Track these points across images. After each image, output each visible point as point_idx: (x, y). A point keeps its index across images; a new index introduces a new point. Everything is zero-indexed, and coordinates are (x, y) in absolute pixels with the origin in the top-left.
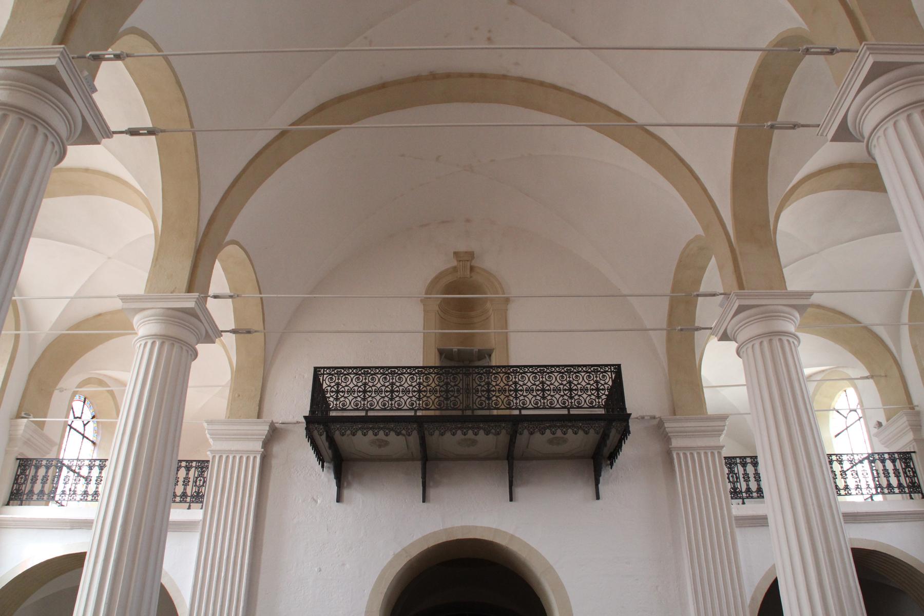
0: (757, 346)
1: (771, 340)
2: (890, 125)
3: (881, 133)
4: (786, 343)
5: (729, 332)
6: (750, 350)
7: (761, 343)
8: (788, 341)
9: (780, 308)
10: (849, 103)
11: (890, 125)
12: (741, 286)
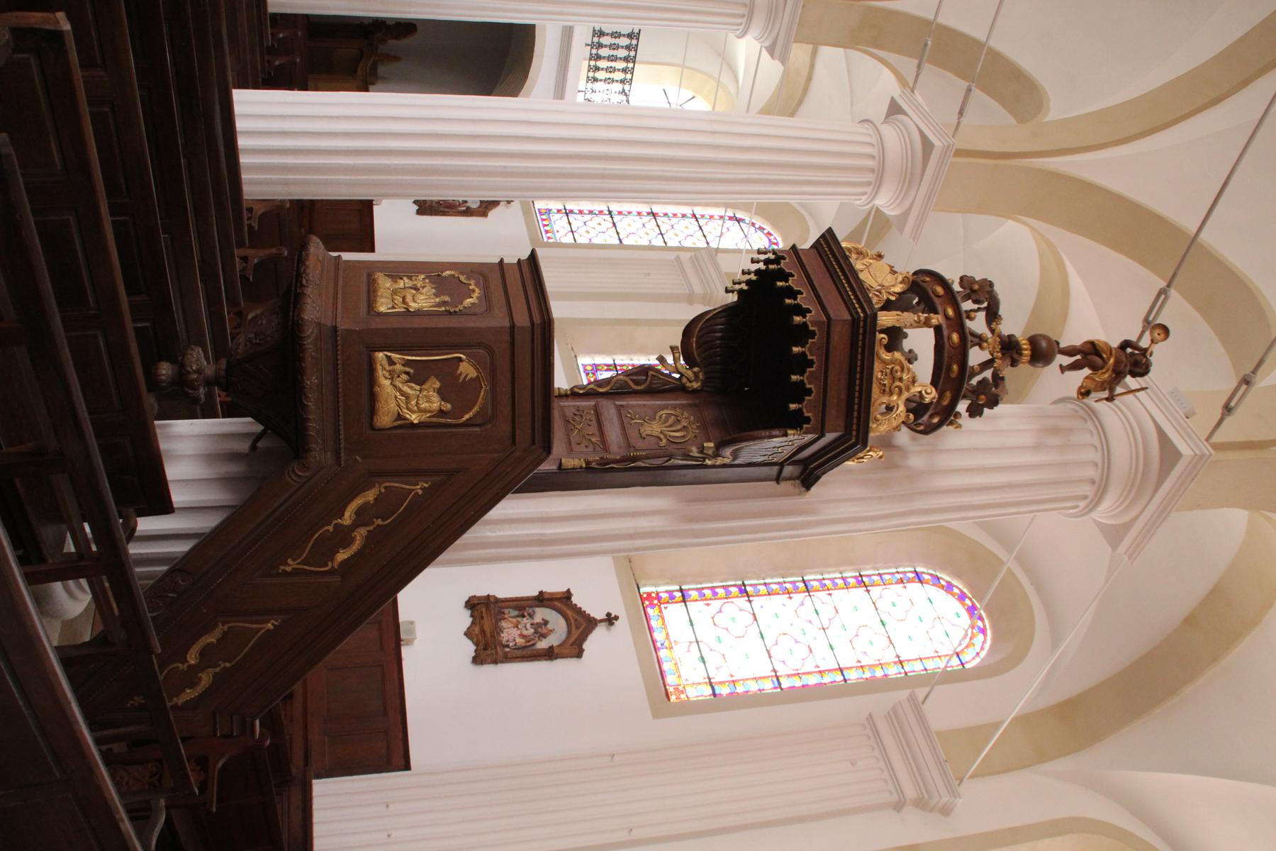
0: (869, 150)
1: (873, 171)
2: (874, 141)
3: (871, 132)
4: (739, 21)
5: (901, 117)
6: (868, 139)
7: (873, 157)
8: (865, 194)
9: (777, 26)
10: (914, 119)
11: (874, 141)
12: (960, 153)
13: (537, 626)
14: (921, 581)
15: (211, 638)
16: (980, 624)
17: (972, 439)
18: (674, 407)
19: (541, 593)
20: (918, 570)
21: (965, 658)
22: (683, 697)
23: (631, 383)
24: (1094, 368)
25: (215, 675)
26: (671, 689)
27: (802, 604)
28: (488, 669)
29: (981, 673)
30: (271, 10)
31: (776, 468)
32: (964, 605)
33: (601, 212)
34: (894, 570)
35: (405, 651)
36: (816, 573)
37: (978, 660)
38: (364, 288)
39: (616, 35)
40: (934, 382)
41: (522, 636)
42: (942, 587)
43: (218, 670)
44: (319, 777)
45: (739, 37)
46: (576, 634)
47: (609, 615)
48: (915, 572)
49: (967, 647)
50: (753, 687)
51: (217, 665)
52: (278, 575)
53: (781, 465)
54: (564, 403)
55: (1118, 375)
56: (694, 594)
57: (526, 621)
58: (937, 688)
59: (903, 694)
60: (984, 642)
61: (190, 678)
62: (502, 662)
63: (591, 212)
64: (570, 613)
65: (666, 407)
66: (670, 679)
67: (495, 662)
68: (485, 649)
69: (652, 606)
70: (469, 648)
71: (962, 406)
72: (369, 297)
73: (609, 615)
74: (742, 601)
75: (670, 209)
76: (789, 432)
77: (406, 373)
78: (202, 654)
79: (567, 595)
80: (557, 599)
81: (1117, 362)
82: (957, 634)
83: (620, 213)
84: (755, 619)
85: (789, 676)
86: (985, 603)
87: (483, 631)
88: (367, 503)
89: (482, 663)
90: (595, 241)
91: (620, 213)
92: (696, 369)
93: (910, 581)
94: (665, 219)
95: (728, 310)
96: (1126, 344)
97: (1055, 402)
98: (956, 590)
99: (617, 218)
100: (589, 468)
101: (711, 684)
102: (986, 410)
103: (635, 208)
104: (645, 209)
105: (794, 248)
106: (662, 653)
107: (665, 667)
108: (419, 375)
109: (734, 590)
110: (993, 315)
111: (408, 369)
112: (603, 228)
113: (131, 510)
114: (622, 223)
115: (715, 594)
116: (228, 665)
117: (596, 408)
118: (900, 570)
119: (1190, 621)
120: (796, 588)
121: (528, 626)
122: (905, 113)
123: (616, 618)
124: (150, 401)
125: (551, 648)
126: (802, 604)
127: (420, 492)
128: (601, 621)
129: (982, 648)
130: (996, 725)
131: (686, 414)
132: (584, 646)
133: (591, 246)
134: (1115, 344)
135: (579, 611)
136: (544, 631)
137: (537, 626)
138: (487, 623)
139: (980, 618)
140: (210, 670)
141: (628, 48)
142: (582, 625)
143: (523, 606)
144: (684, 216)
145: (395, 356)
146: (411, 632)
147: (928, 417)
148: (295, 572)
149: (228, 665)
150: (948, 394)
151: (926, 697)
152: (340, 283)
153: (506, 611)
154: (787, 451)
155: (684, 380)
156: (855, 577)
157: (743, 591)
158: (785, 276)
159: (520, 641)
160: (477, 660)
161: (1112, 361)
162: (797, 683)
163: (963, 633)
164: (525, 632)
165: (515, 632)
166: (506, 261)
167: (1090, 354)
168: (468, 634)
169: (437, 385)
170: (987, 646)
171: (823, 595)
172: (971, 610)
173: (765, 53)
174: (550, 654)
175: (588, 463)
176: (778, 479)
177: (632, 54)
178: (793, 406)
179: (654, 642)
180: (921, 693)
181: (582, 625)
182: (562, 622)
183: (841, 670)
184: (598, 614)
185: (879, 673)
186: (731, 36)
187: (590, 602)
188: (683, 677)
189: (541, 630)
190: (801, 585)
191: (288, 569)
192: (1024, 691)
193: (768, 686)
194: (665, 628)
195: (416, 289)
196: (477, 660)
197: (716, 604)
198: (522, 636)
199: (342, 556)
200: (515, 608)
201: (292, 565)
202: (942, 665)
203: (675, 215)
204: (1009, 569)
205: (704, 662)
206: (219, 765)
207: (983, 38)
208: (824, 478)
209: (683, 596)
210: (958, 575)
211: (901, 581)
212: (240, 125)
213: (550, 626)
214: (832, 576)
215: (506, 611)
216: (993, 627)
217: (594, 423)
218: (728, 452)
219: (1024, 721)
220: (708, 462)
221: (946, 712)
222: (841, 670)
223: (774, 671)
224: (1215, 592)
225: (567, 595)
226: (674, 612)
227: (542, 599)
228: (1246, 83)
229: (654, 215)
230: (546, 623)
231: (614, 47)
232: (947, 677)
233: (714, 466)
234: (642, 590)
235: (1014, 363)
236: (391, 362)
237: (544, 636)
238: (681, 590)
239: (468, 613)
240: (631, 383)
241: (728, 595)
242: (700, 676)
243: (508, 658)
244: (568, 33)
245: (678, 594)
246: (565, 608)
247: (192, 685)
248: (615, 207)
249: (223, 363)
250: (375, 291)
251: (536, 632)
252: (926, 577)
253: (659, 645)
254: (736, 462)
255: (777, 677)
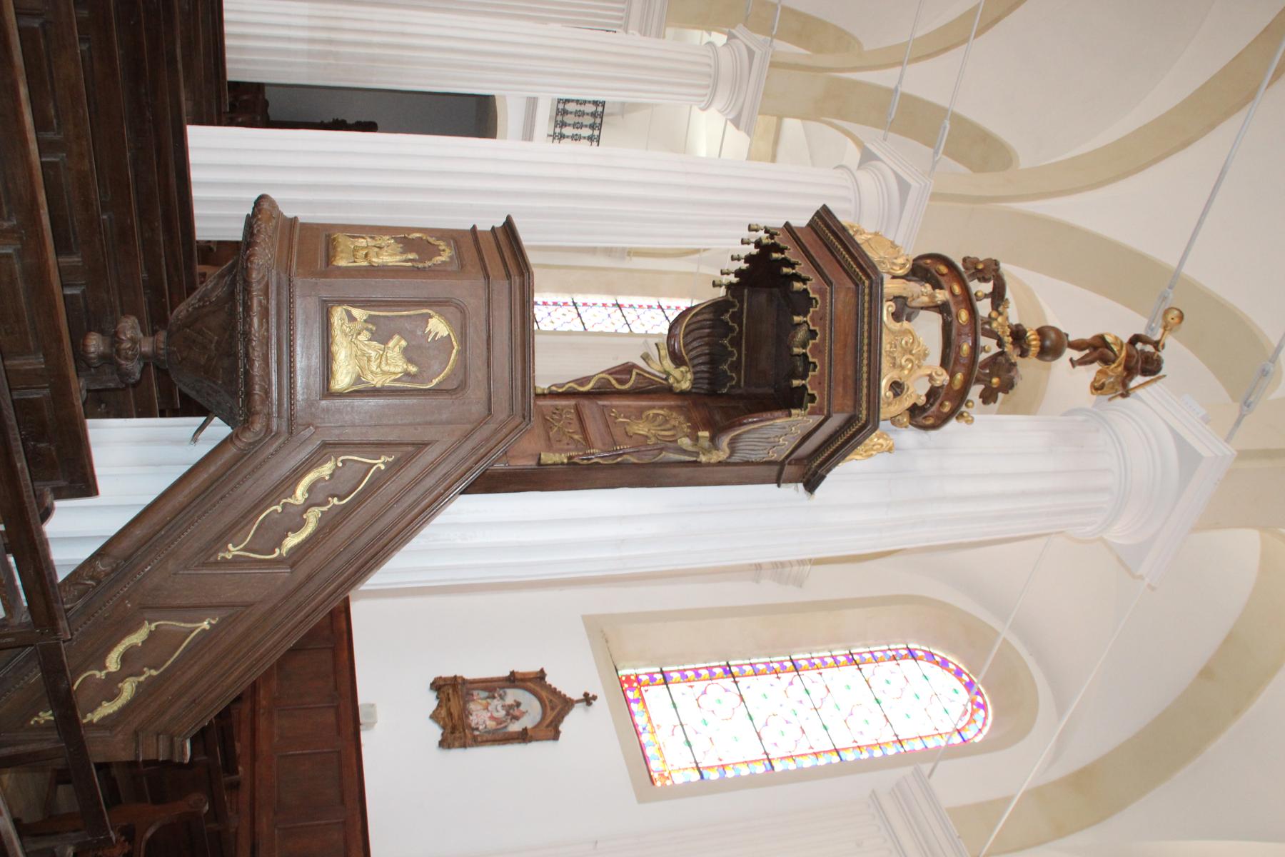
4: (703, 92)
13: (509, 709)
14: (914, 658)
15: (137, 638)
16: (979, 699)
17: (983, 433)
18: (662, 408)
19: (512, 673)
20: (911, 646)
21: (968, 734)
22: (669, 783)
23: (614, 382)
24: (1106, 361)
25: (139, 684)
26: (655, 776)
27: (791, 683)
28: (457, 754)
29: (988, 746)
30: (231, 77)
31: (776, 468)
32: (961, 681)
33: (565, 304)
34: (885, 647)
35: (365, 736)
36: (804, 652)
37: (980, 737)
38: (322, 246)
39: (576, 138)
40: (944, 363)
41: (492, 718)
42: (937, 663)
43: (142, 679)
44: (237, 242)
45: (704, 109)
46: (551, 715)
47: (586, 695)
48: (908, 649)
49: (968, 723)
50: (745, 771)
51: (142, 673)
52: (217, 563)
53: (781, 464)
54: (541, 403)
55: (1130, 371)
56: (676, 676)
57: (496, 703)
58: (941, 764)
59: (908, 770)
60: (985, 718)
61: (109, 689)
62: (471, 746)
63: (555, 304)
64: (544, 694)
65: (653, 407)
66: (655, 765)
67: (464, 746)
68: (452, 733)
69: (632, 689)
70: (436, 732)
71: (976, 391)
72: (327, 250)
73: (586, 695)
74: (728, 682)
75: (636, 300)
76: (793, 411)
77: (367, 329)
78: (124, 658)
79: (541, 675)
80: (530, 680)
81: (1129, 356)
82: (956, 710)
83: (585, 304)
84: (742, 699)
85: (782, 758)
86: (981, 676)
87: (450, 714)
88: (321, 479)
89: (449, 747)
90: (559, 329)
91: (585, 304)
92: (683, 369)
93: (902, 658)
94: (631, 310)
95: (717, 307)
96: (1135, 339)
97: (1065, 414)
98: (951, 666)
99: (581, 310)
100: (571, 463)
101: (698, 769)
102: (1001, 395)
103: (600, 299)
104: (610, 300)
105: (787, 225)
106: (645, 738)
107: (649, 752)
108: (381, 335)
109: (718, 671)
110: (998, 297)
111: (370, 326)
112: (568, 318)
113: (47, 490)
114: (587, 314)
115: (698, 675)
116: (154, 673)
117: (577, 408)
118: (892, 647)
119: (1207, 673)
120: (784, 668)
121: (499, 708)
122: (878, 159)
123: (595, 698)
124: (79, 388)
125: (525, 730)
126: (791, 683)
127: (383, 467)
128: (578, 701)
129: (984, 724)
130: (1008, 800)
131: (675, 415)
132: (561, 728)
133: (555, 332)
134: (1126, 340)
135: (554, 692)
136: (516, 713)
137: (509, 709)
138: (455, 707)
139: (979, 693)
140: (131, 679)
141: (592, 127)
142: (556, 707)
143: (492, 687)
144: (649, 307)
145: (356, 312)
146: (372, 715)
147: (933, 412)
148: (236, 561)
149: (154, 673)
150: (959, 376)
151: (932, 771)
152: (296, 240)
153: (475, 693)
154: (786, 445)
155: (671, 380)
156: (846, 656)
157: (728, 671)
158: (777, 248)
159: (491, 724)
160: (445, 744)
161: (1124, 354)
162: (791, 766)
163: (962, 709)
164: (496, 715)
165: (486, 715)
166: (479, 228)
167: (1097, 349)
168: (434, 717)
169: (403, 343)
170: (989, 721)
171: (813, 674)
172: (969, 685)
173: (730, 127)
174: (524, 737)
175: (570, 458)
176: (778, 481)
177: (596, 133)
178: (796, 383)
179: (635, 726)
180: (926, 768)
181: (556, 707)
182: (536, 704)
183: (837, 751)
184: (574, 693)
185: (877, 753)
186: (695, 108)
187: (564, 681)
188: (669, 762)
189: (513, 712)
190: (789, 665)
191: (229, 556)
192: (1030, 765)
193: (760, 769)
194: (647, 711)
195: (380, 248)
196: (445, 744)
197: (699, 686)
198: (492, 718)
199: (292, 541)
200: (485, 689)
201: (233, 551)
202: (943, 744)
203: (640, 306)
204: (1005, 640)
205: (690, 746)
206: (148, 835)
207: (947, 106)
208: (829, 477)
209: (664, 678)
210: (953, 651)
211: (894, 658)
212: (195, 175)
213: (522, 708)
214: (821, 654)
215: (475, 693)
216: (993, 702)
217: (575, 421)
218: (725, 441)
219: (1038, 794)
220: (703, 459)
221: (958, 787)
222: (837, 751)
223: (766, 753)
224: (1230, 639)
225: (541, 675)
226: (656, 695)
227: (514, 680)
228: (1211, 127)
229: (620, 307)
230: (518, 704)
231: (578, 126)
232: (950, 752)
233: (709, 464)
234: (620, 673)
235: (1023, 354)
236: (352, 319)
237: (516, 718)
238: (662, 672)
239: (434, 694)
240: (614, 382)
241: (712, 676)
242: (687, 761)
243: (477, 741)
244: (532, 103)
245: (659, 677)
246: (537, 689)
247: (112, 697)
248: (579, 299)
249: (162, 336)
250: (335, 248)
251: (508, 714)
252: (920, 654)
253: (640, 729)
254: (733, 459)
255: (770, 761)
